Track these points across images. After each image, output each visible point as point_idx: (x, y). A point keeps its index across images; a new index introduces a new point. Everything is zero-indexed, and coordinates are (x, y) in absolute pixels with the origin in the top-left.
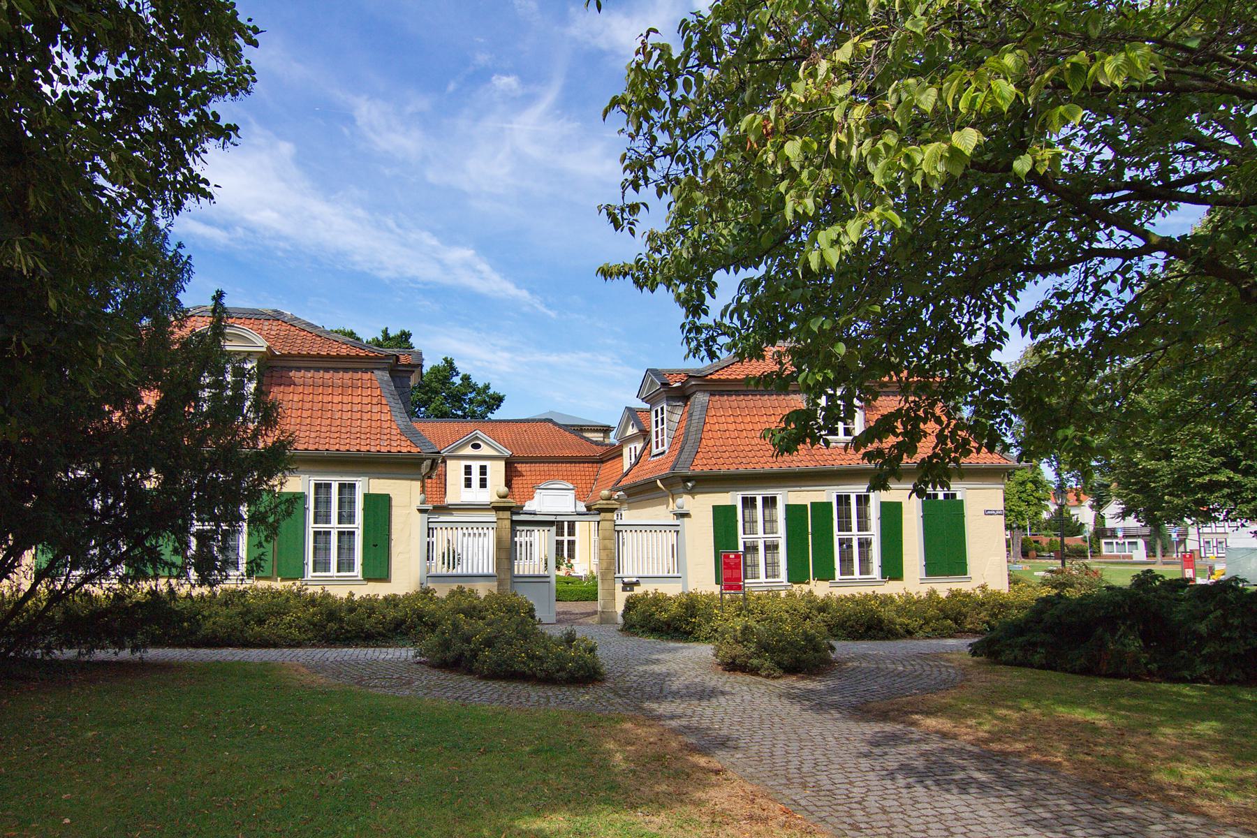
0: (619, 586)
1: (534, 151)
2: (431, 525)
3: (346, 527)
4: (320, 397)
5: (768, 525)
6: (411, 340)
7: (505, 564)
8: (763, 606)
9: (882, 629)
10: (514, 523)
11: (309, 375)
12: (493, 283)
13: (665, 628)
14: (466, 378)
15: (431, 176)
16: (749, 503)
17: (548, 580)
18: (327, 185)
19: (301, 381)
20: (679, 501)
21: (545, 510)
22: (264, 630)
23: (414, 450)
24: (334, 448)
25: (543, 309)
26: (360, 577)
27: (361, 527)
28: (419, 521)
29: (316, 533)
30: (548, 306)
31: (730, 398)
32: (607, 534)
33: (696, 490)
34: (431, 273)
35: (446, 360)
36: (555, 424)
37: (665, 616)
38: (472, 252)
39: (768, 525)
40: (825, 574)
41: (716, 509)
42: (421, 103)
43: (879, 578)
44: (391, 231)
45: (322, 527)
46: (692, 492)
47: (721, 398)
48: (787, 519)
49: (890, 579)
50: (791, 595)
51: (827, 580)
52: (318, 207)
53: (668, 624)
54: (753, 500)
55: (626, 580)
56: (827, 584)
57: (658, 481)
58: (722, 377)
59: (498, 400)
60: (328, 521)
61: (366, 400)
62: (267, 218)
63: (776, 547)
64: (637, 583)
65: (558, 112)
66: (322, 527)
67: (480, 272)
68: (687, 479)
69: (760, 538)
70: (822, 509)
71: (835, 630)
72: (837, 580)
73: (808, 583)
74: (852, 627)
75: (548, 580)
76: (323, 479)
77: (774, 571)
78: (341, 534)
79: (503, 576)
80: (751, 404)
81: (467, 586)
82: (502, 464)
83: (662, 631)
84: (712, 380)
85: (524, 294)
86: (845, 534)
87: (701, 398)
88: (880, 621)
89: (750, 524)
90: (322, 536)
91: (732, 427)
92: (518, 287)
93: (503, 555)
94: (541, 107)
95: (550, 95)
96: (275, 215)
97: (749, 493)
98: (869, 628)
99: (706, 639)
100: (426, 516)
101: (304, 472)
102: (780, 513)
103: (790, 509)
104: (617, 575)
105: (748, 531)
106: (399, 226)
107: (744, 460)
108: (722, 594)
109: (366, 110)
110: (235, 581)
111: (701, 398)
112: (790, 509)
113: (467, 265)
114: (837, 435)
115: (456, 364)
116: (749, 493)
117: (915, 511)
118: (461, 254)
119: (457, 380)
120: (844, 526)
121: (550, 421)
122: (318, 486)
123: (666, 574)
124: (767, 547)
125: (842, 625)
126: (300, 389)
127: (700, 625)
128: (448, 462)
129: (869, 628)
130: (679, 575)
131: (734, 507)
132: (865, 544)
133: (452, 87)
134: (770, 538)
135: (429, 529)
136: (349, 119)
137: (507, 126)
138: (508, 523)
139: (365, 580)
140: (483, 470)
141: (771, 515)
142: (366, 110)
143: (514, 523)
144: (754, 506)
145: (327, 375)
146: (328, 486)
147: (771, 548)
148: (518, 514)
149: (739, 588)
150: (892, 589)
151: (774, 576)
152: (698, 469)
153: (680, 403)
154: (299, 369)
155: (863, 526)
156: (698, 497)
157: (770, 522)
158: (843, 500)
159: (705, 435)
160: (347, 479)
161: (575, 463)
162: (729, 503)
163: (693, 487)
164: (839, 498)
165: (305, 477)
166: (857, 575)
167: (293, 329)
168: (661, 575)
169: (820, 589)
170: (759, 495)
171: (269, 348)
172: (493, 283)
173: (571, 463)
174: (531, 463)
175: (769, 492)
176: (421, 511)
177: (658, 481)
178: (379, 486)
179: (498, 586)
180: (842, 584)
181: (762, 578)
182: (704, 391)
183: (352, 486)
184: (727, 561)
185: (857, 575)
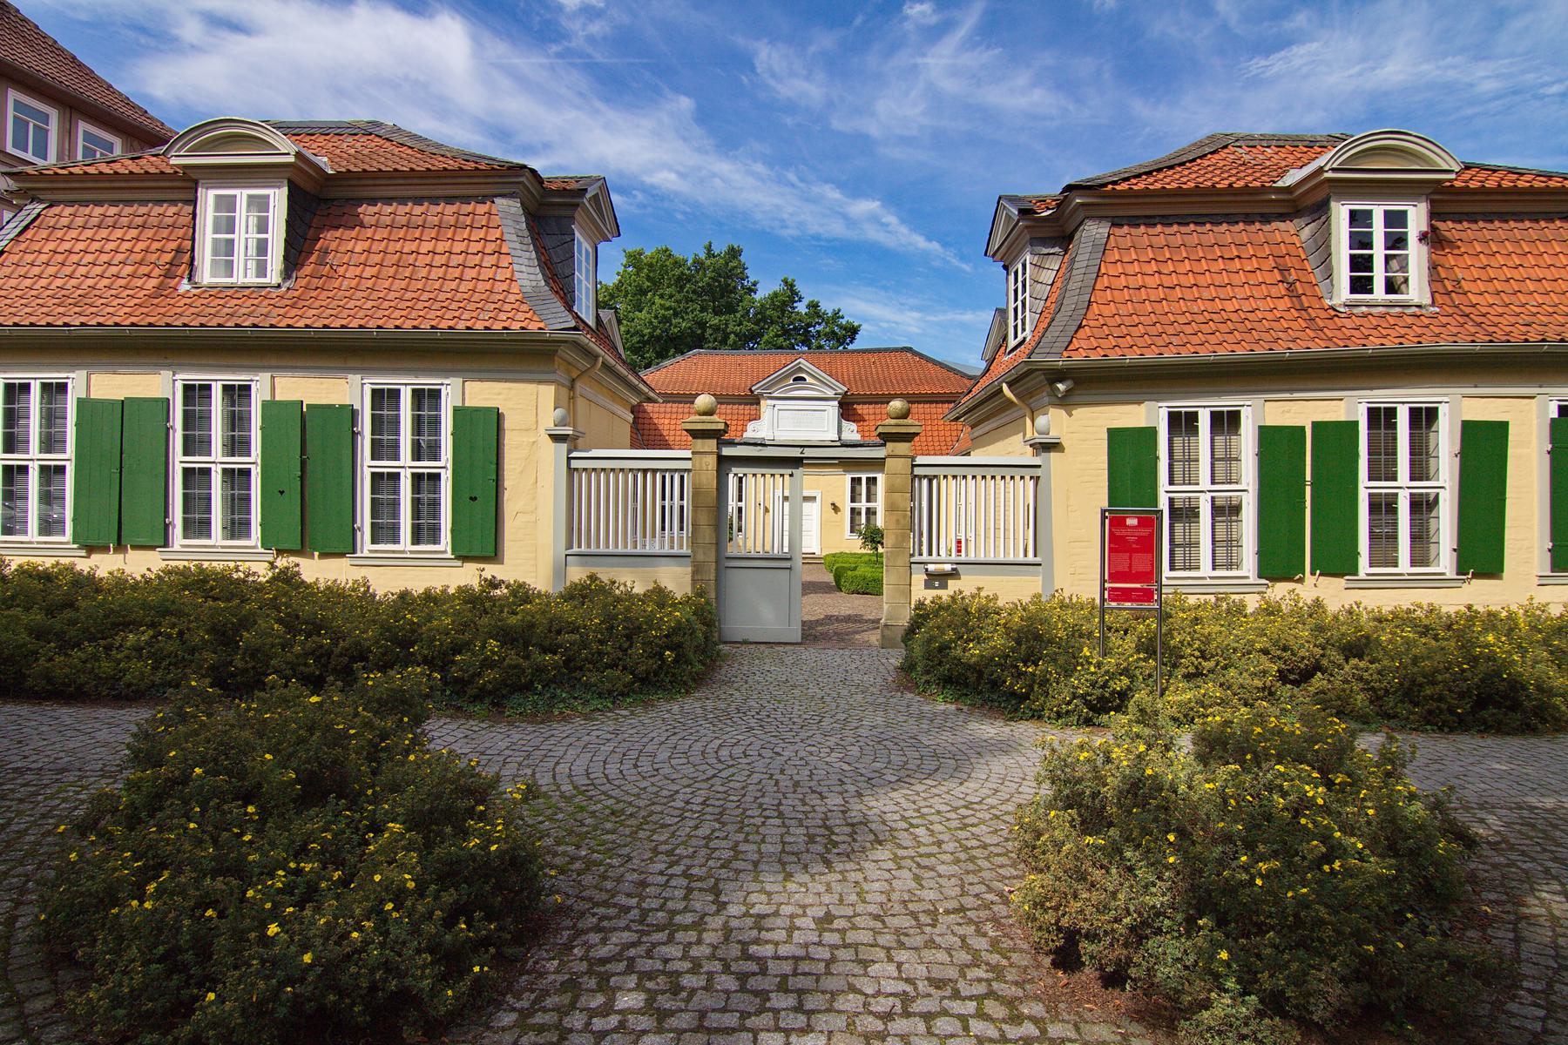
0: (919, 578)
1: (949, 86)
2: (574, 464)
3: (426, 466)
4: (398, 246)
5: (1221, 552)
6: (743, 259)
8: (1207, 639)
9: (1515, 706)
10: (724, 463)
11: (389, 209)
12: (900, 235)
13: (972, 678)
14: (814, 306)
15: (836, 124)
16: (1182, 424)
17: (787, 564)
18: (727, 144)
19: (373, 220)
20: (1041, 421)
21: (783, 436)
22: (61, 665)
25: (955, 262)
27: (450, 466)
28: (553, 455)
30: (963, 258)
31: (1151, 231)
32: (898, 481)
33: (1077, 399)
34: (837, 229)
35: (785, 282)
36: (915, 353)
37: (975, 651)
38: (877, 204)
39: (1220, 465)
40: (1338, 563)
41: (1114, 435)
42: (825, 40)
43: (1450, 573)
44: (793, 186)
45: (385, 466)
46: (1066, 402)
47: (1133, 231)
49: (1475, 576)
50: (1271, 610)
51: (342, 555)
52: (724, 167)
53: (978, 670)
54: (1193, 417)
55: (931, 567)
56: (1340, 582)
57: (1005, 386)
59: (853, 331)
60: (435, 456)
61: (475, 247)
62: (666, 179)
63: (1236, 509)
64: (954, 574)
65: (978, 38)
66: (385, 466)
67: (887, 225)
68: (1057, 375)
70: (1336, 436)
71: (1390, 701)
72: (1362, 575)
73: (1301, 581)
74: (1441, 699)
75: (787, 564)
76: (386, 381)
77: (1229, 555)
78: (417, 478)
79: (701, 557)
80: (1195, 239)
81: (605, 575)
83: (967, 685)
84: (1114, 192)
85: (935, 246)
86: (1383, 487)
87: (1094, 231)
88: (1516, 685)
89: (1183, 467)
91: (1152, 282)
92: (929, 239)
94: (962, 32)
95: (969, 20)
96: (673, 177)
97: (1184, 405)
98: (1481, 703)
99: (1059, 715)
100: (564, 447)
101: (355, 370)
102: (1247, 442)
103: (1269, 437)
104: (916, 558)
105: (1178, 477)
106: (802, 180)
107: (1175, 340)
109: (768, 56)
110: (864, 477)
111: (1094, 231)
112: (1269, 437)
113: (874, 219)
114: (1371, 291)
115: (798, 287)
116: (1184, 405)
117: (1535, 441)
118: (865, 207)
119: (801, 308)
120: (1383, 468)
121: (909, 350)
122: (377, 395)
123: (1021, 558)
124: (1217, 510)
125: (1410, 691)
126: (369, 232)
127: (1044, 682)
128: (762, 402)
129: (1481, 703)
130: (1038, 560)
131: (1152, 432)
132: (236, 478)
133: (858, 21)
134: (1224, 492)
135: (571, 471)
136: (745, 62)
137: (920, 61)
138: (711, 461)
139: (458, 558)
141: (1228, 448)
142: (768, 56)
144: (1193, 430)
145: (418, 210)
146: (395, 394)
147: (1226, 511)
148: (732, 443)
149: (1147, 595)
150: (1481, 595)
151: (1229, 566)
153: (1057, 250)
154: (373, 201)
155: (1420, 470)
156: (1079, 412)
157: (1224, 462)
158: (1381, 418)
159: (1099, 296)
160: (54, 376)
161: (937, 402)
163: (1068, 392)
164: (1373, 414)
165: (355, 379)
166: (1404, 565)
167: (388, 144)
168: (1011, 558)
169: (1332, 594)
170: (1204, 409)
171: (298, 155)
172: (900, 235)
173: (931, 402)
174: (876, 403)
175: (1225, 403)
176: (556, 438)
177: (1005, 386)
178: (483, 393)
179: (694, 573)
180: (1373, 583)
181: (1206, 569)
182: (1101, 218)
183: (435, 395)
184: (1118, 532)
185: (1404, 565)
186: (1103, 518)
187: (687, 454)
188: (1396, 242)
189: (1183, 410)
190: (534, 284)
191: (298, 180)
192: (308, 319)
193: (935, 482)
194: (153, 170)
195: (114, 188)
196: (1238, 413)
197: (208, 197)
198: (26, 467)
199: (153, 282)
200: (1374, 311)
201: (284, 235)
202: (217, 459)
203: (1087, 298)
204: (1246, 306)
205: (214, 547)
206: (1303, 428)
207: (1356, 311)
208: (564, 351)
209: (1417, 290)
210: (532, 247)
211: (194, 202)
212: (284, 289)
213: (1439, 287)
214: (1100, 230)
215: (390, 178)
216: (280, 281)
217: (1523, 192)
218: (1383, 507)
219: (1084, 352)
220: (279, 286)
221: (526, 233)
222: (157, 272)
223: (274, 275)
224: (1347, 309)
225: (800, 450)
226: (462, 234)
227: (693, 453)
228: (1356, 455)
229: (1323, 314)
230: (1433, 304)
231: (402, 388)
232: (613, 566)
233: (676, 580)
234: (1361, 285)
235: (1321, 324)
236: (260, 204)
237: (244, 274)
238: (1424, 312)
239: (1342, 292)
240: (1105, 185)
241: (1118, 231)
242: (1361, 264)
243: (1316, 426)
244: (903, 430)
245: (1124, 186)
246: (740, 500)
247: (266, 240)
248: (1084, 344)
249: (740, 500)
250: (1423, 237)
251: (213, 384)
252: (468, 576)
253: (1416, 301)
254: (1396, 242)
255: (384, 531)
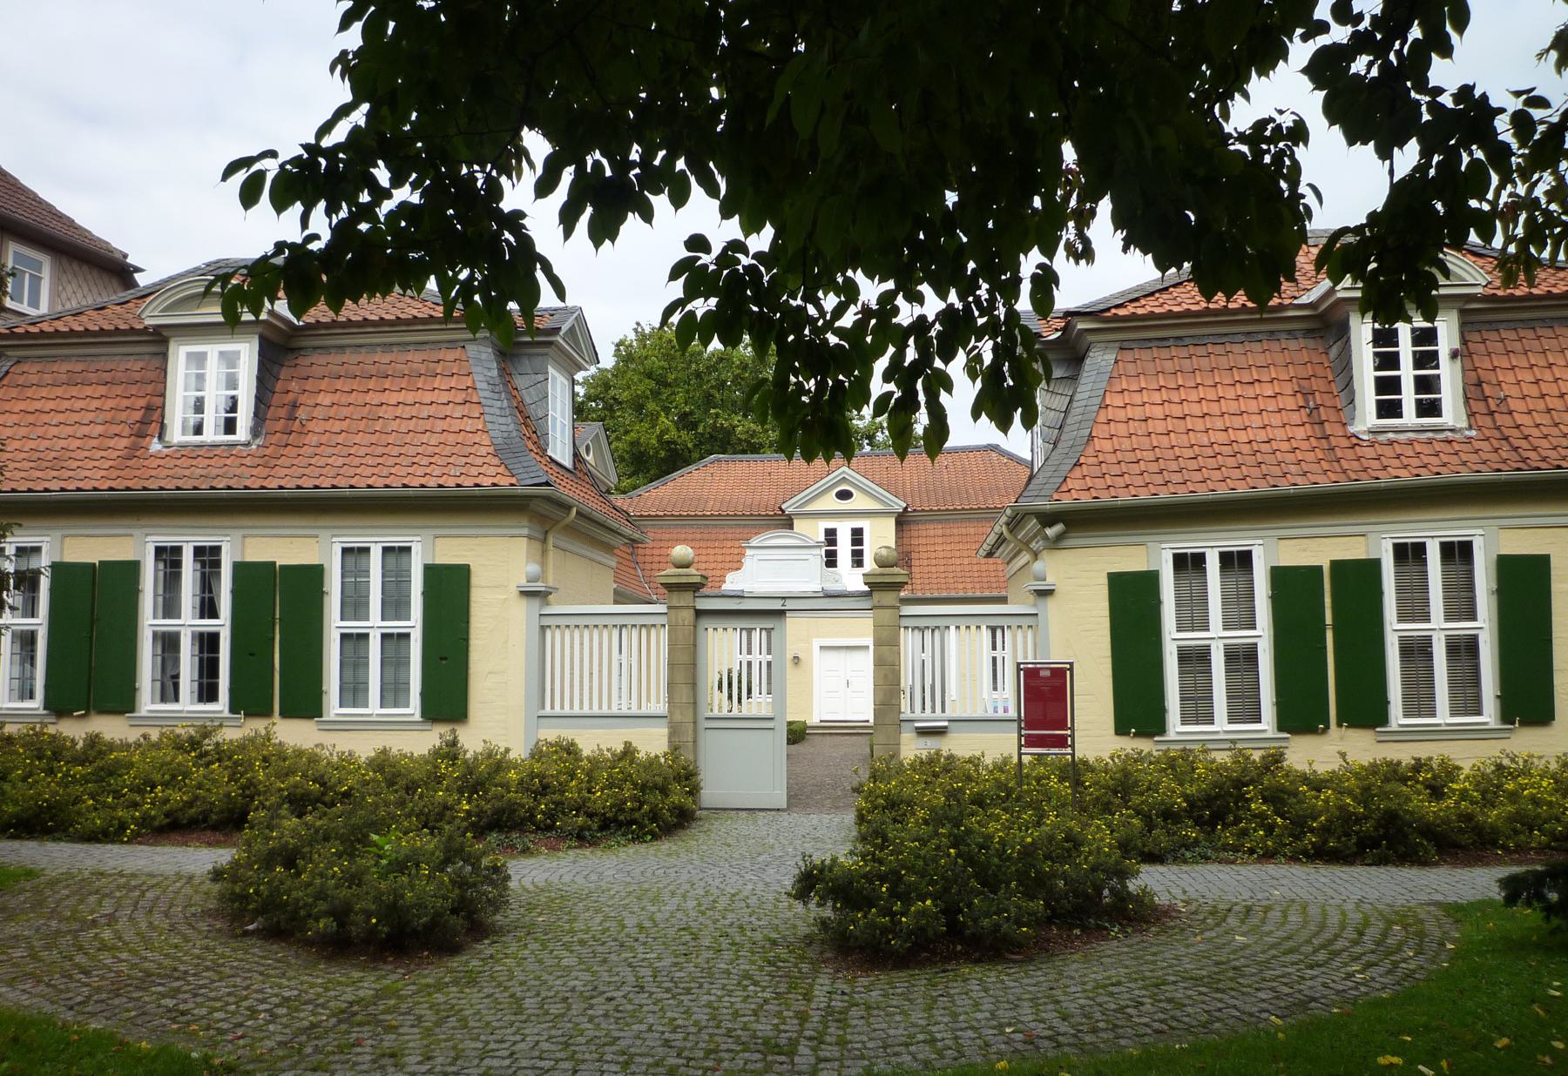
2: (546, 621)
3: (395, 626)
7: (684, 694)
23: (504, 481)
24: (416, 482)
26: (418, 717)
27: (228, 623)
28: (522, 614)
29: (344, 637)
40: (305, 703)
45: (354, 626)
48: (1276, 599)
51: (311, 717)
58: (1140, 311)
68: (1047, 519)
69: (1217, 636)
79: (678, 717)
82: (891, 522)
84: (1116, 318)
86: (1415, 628)
87: (1100, 360)
90: (168, 644)
93: (681, 677)
103: (1280, 576)
108: (1020, 755)
112: (1280, 576)
114: (1400, 416)
132: (1463, 650)
135: (543, 628)
138: (688, 615)
140: (857, 537)
143: (699, 613)
152: (1066, 501)
160: (396, 540)
162: (1143, 568)
163: (1060, 537)
166: (1443, 716)
170: (1211, 545)
180: (1407, 735)
183: (216, 550)
185: (1443, 716)
186: (1019, 670)
187: (662, 608)
188: (1425, 359)
189: (1189, 551)
190: (505, 435)
191: (268, 334)
192: (285, 479)
193: (999, 633)
194: (123, 327)
195: (1543, 307)
196: (1250, 553)
197: (180, 354)
198: (367, 635)
199: (124, 442)
200: (1402, 437)
201: (254, 391)
202: (188, 622)
203: (1087, 432)
204: (1262, 436)
205: (371, 715)
206: (1320, 568)
207: (1381, 438)
208: (533, 505)
209: (1452, 412)
210: (503, 395)
211: (164, 356)
212: (254, 447)
213: (1479, 407)
214: (1106, 357)
215: (408, 325)
216: (249, 437)
217: (1539, 298)
218: (1417, 651)
219: (1077, 495)
220: (248, 444)
221: (497, 381)
222: (127, 432)
223: (242, 433)
224: (1370, 437)
225: (782, 602)
226: (433, 382)
227: (669, 608)
228: (234, 592)
229: (1345, 443)
230: (1470, 427)
231: (184, 545)
232: (592, 727)
233: (652, 743)
234: (1389, 409)
235: (1340, 454)
236: (230, 360)
237: (212, 434)
238: (1457, 436)
239: (1366, 417)
240: (1108, 309)
241: (1128, 356)
242: (1388, 386)
243: (1336, 565)
244: (684, 580)
245: (1130, 310)
246: (994, 659)
247: (203, 398)
248: (1077, 484)
249: (994, 659)
250: (1454, 355)
251: (184, 545)
252: (421, 742)
253: (243, 439)
254: (1425, 359)
255: (353, 691)
